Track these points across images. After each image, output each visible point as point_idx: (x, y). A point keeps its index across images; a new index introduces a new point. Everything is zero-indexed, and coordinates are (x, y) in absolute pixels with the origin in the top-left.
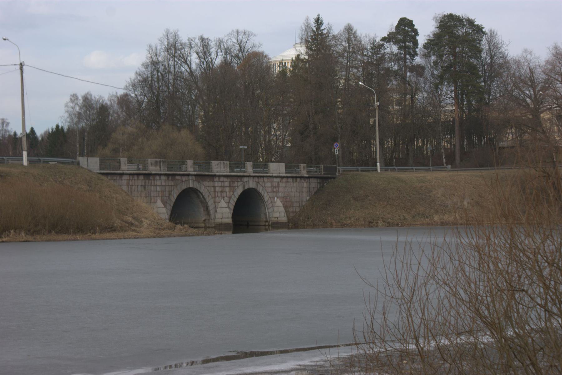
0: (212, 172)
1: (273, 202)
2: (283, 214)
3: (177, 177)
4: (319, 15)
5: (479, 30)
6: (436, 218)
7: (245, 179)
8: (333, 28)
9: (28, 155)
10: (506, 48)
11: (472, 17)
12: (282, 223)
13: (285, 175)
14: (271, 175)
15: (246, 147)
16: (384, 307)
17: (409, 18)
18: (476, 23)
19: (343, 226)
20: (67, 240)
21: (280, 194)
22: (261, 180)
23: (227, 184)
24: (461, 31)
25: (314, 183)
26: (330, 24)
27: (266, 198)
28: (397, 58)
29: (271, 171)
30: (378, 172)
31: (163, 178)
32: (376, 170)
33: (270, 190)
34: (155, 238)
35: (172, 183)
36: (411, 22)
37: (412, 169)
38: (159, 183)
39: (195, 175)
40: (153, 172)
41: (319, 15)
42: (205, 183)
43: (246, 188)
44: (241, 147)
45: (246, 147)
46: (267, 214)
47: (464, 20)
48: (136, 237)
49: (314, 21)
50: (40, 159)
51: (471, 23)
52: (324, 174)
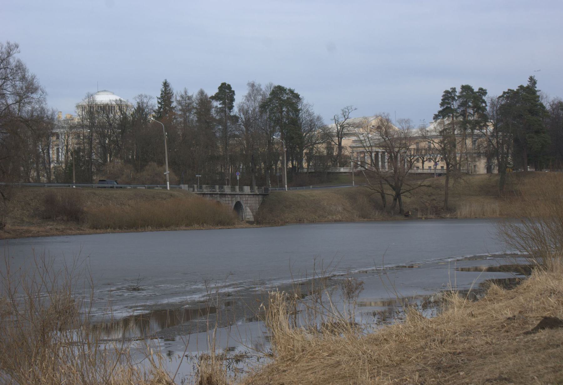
0: (255, 192)
1: (246, 209)
2: (252, 217)
3: (214, 195)
4: (166, 80)
5: (297, 96)
6: (330, 218)
7: (236, 196)
8: (188, 91)
9: (170, 185)
10: (312, 108)
11: (292, 88)
12: (252, 221)
13: (250, 193)
14: (245, 193)
15: (201, 176)
16: (332, 261)
17: (227, 83)
18: (295, 92)
19: (285, 223)
20: (103, 233)
21: (249, 205)
22: (242, 196)
23: (230, 199)
24: (285, 97)
25: (260, 198)
26: (186, 88)
27: (244, 207)
28: (221, 110)
29: (245, 191)
30: (167, 189)
31: (209, 196)
32: (285, 190)
33: (245, 202)
34: (151, 232)
35: (211, 199)
36: (229, 86)
37: (297, 189)
38: (227, 199)
39: (220, 194)
40: (206, 193)
41: (166, 80)
42: (223, 198)
43: (237, 201)
44: (197, 176)
45: (201, 176)
46: (244, 216)
47: (287, 90)
48: (81, 234)
49: (163, 84)
50: (93, 186)
51: (292, 92)
52: (265, 193)
